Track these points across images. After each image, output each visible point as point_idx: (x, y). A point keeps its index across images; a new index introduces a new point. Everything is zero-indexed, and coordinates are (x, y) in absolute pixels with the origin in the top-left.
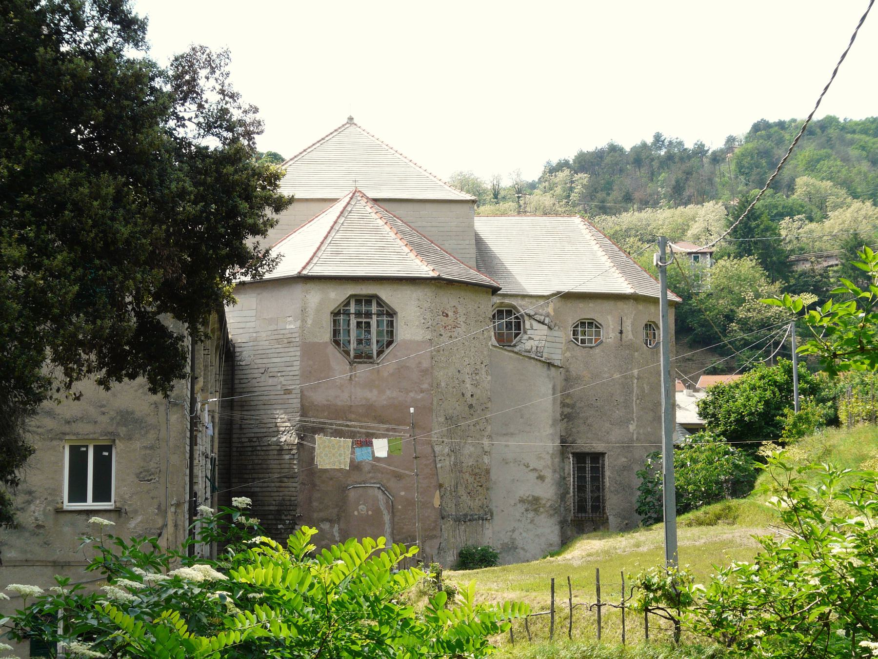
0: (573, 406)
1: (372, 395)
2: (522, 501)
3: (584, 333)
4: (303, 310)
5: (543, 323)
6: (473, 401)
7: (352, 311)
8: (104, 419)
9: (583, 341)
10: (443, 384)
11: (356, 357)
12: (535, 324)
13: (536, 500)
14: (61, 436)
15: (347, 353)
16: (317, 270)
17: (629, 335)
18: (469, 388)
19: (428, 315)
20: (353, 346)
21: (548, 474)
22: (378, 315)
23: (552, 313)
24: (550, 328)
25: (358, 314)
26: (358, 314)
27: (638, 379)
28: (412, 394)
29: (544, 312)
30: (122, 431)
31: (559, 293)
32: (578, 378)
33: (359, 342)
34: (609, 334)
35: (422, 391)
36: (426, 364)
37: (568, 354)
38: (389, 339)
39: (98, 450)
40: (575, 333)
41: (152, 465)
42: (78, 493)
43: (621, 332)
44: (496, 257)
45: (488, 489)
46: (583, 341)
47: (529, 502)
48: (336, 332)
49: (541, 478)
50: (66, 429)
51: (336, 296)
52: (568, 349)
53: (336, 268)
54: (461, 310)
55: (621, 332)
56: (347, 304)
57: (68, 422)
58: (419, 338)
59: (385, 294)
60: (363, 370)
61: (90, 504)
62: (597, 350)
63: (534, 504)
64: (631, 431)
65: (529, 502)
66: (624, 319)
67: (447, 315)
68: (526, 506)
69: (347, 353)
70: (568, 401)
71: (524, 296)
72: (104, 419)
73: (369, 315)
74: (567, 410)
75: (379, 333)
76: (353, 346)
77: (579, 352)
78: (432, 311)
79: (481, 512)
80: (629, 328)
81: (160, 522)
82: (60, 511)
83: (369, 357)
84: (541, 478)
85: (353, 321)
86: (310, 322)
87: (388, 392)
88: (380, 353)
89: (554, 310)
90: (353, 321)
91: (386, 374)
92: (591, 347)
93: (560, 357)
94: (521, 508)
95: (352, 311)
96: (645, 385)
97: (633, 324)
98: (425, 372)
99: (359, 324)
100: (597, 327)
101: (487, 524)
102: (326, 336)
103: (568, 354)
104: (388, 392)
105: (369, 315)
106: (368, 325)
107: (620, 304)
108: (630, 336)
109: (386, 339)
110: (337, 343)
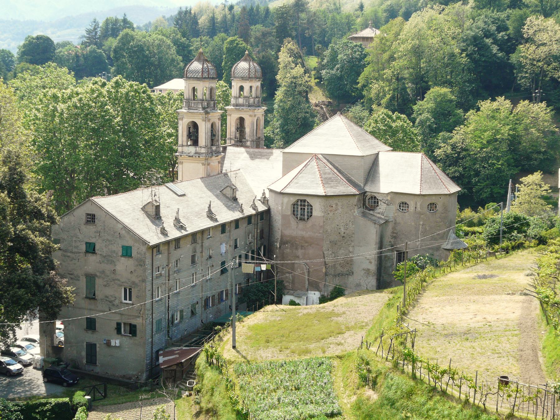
0: (397, 233)
1: (303, 233)
2: (364, 270)
3: (403, 207)
4: (282, 203)
5: (385, 203)
6: (345, 235)
7: (299, 204)
8: (130, 283)
9: (402, 210)
10: (329, 231)
11: (300, 220)
12: (382, 203)
13: (368, 270)
14: (121, 286)
15: (297, 218)
16: (288, 191)
17: (419, 209)
18: (342, 230)
19: (323, 208)
20: (299, 216)
21: (373, 261)
22: (307, 206)
23: (390, 199)
24: (388, 205)
25: (301, 205)
26: (301, 205)
27: (422, 225)
28: (317, 234)
29: (386, 199)
30: (133, 286)
31: (392, 192)
32: (399, 223)
33: (301, 215)
34: (412, 209)
35: (320, 233)
36: (322, 224)
37: (396, 214)
38: (310, 215)
39: (130, 289)
40: (400, 206)
41: (139, 295)
42: (125, 299)
43: (416, 208)
44: (379, 173)
45: (351, 265)
46: (402, 210)
47: (366, 270)
48: (294, 211)
49: (371, 262)
50: (122, 284)
51: (293, 200)
52: (396, 212)
53: (297, 190)
54: (339, 204)
55: (416, 208)
56: (298, 202)
57: (122, 283)
58: (319, 215)
59: (308, 199)
60: (301, 224)
61: (128, 301)
62: (407, 214)
63: (368, 271)
64: (417, 244)
65: (366, 270)
66: (417, 203)
67: (332, 207)
68: (365, 271)
69: (297, 218)
70: (395, 231)
71: (379, 193)
72: (130, 283)
73: (304, 206)
74: (395, 235)
75: (308, 212)
76: (299, 216)
77: (400, 214)
78: (324, 206)
79: (347, 273)
80: (419, 207)
81: (141, 308)
82: (121, 303)
83: (305, 220)
84: (371, 262)
85: (299, 208)
86: (284, 208)
87: (309, 233)
88: (308, 219)
89: (391, 198)
90: (299, 208)
91: (308, 227)
92: (405, 212)
93: (392, 215)
94: (363, 272)
95: (299, 204)
96: (427, 227)
97: (421, 205)
98: (321, 227)
99: (301, 209)
100: (408, 205)
101: (350, 277)
102: (289, 212)
103: (396, 214)
104: (309, 233)
105: (304, 206)
106: (304, 209)
107: (416, 197)
108: (419, 209)
109: (310, 214)
110: (294, 214)
